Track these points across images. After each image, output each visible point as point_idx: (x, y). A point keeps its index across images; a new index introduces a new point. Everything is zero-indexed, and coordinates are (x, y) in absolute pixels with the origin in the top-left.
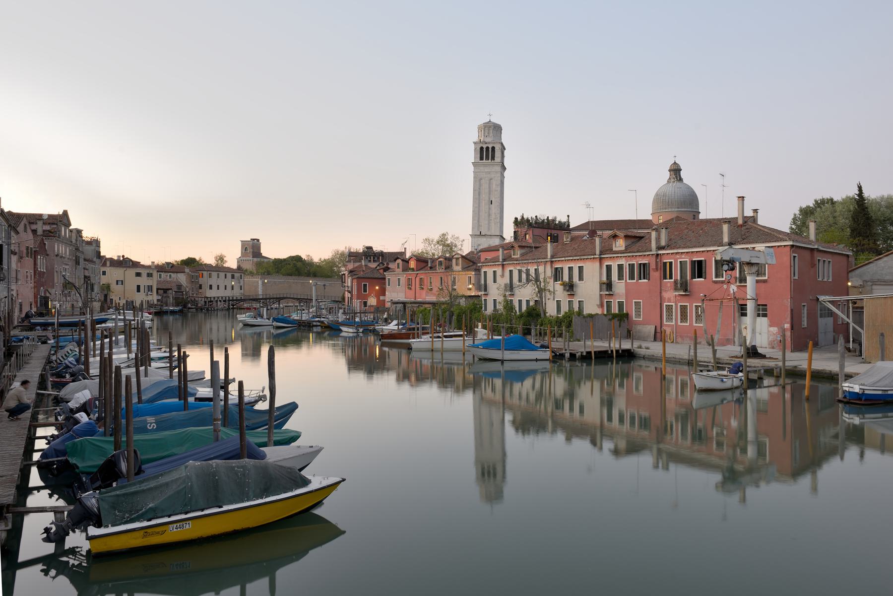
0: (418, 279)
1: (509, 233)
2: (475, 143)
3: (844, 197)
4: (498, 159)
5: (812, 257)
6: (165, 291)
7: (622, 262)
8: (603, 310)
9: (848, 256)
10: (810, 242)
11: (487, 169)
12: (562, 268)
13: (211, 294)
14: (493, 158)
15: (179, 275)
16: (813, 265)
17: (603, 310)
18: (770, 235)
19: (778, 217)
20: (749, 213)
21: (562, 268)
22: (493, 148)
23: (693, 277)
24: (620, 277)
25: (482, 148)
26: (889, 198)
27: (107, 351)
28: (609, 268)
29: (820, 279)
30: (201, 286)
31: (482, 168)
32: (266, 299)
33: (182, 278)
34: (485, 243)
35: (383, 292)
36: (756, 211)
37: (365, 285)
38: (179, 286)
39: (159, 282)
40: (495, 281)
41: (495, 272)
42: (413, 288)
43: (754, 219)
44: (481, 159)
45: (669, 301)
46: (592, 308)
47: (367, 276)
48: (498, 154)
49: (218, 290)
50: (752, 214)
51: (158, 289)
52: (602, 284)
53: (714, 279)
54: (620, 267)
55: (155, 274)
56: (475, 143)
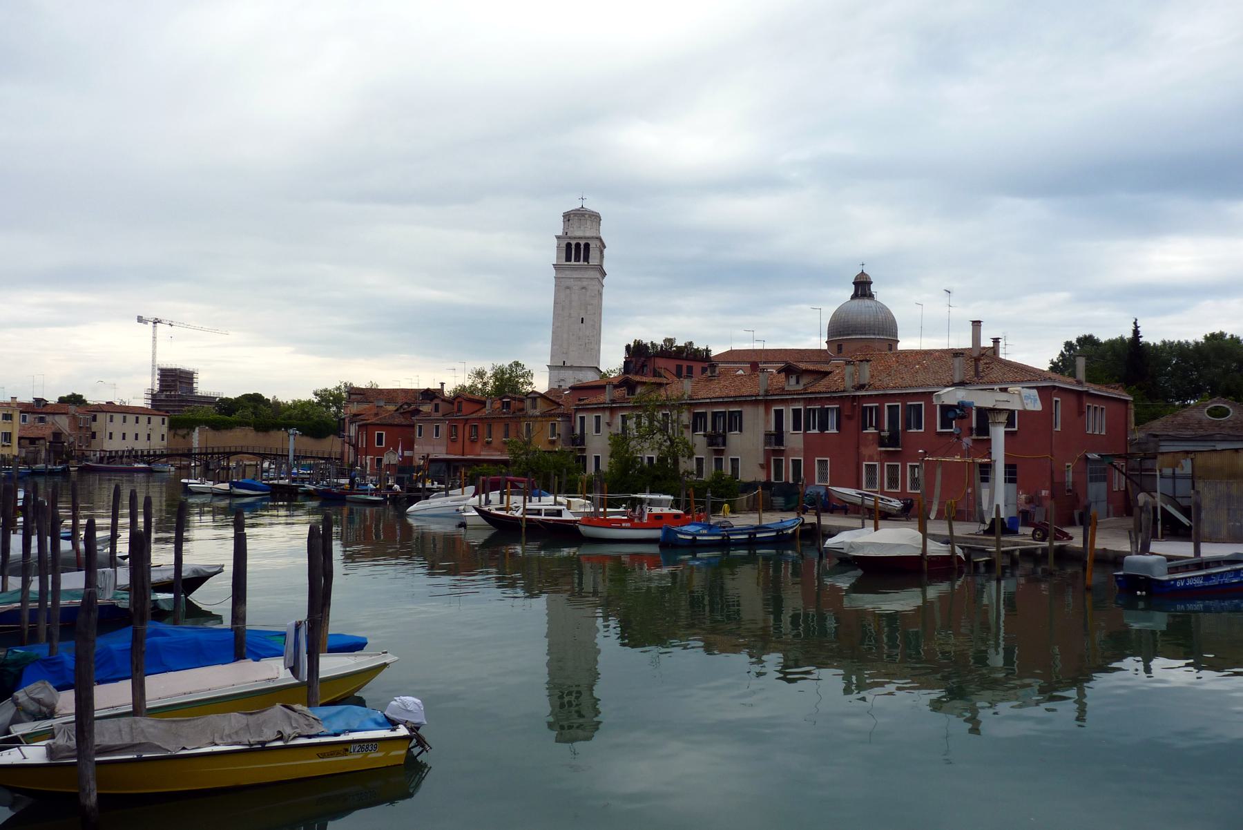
0: (467, 428)
1: (612, 360)
2: (558, 237)
3: (1183, 340)
4: (593, 261)
5: (1080, 405)
6: (33, 441)
7: (800, 406)
8: (768, 475)
9: (1126, 402)
10: (1079, 383)
11: (576, 274)
12: (705, 413)
13: (116, 445)
14: (586, 259)
15: (57, 418)
16: (1081, 413)
17: (768, 475)
18: (1022, 373)
19: (1039, 353)
20: (986, 343)
21: (705, 413)
22: (587, 246)
23: (908, 425)
24: (796, 427)
25: (569, 245)
26: (1234, 340)
27: (141, 520)
28: (779, 414)
29: (1090, 432)
30: (94, 435)
31: (568, 273)
32: (206, 454)
33: (63, 423)
34: (571, 379)
35: (409, 445)
36: (996, 341)
37: (380, 436)
38: (57, 435)
39: (22, 429)
40: (598, 430)
41: (598, 418)
42: (460, 439)
43: (995, 349)
44: (568, 259)
45: (871, 459)
46: (751, 472)
47: (384, 422)
48: (593, 253)
49: (116, 439)
50: (991, 345)
51: (20, 438)
52: (768, 435)
53: (939, 430)
54: (796, 413)
55: (17, 416)
56: (558, 237)
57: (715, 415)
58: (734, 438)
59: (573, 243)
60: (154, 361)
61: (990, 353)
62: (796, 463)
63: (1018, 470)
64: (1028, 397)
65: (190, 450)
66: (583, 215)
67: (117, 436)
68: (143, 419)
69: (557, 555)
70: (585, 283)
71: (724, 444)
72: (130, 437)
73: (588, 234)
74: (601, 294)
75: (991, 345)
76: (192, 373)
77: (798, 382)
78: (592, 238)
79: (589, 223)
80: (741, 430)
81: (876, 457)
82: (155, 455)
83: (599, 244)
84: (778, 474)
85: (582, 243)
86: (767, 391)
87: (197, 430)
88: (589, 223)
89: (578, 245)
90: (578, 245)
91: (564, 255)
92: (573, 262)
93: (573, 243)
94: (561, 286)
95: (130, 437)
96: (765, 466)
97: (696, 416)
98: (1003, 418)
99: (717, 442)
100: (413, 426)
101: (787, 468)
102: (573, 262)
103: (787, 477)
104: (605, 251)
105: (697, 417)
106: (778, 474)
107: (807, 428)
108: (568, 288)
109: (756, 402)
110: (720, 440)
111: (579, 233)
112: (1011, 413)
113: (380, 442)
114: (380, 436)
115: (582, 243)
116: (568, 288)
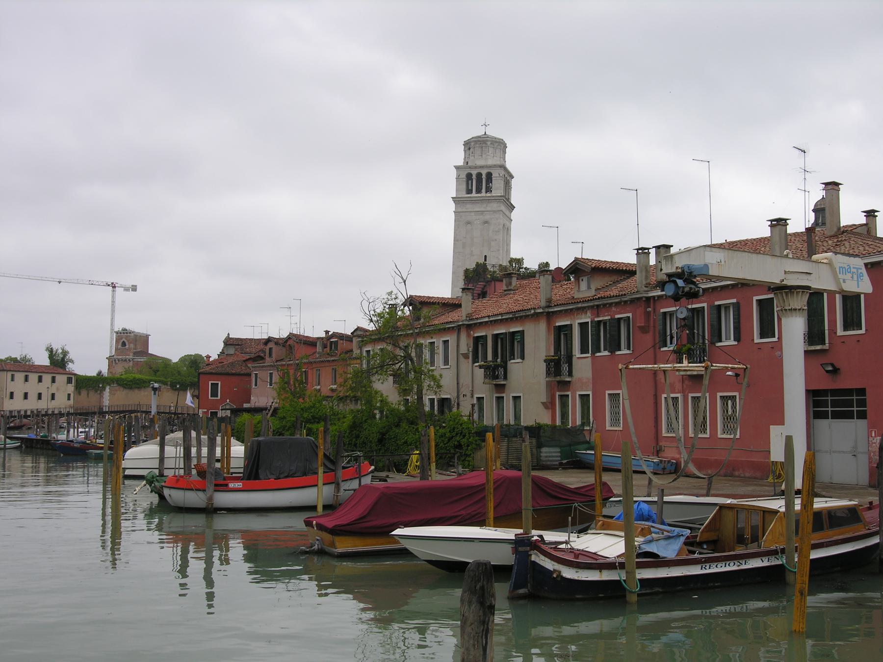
2: (457, 168)
11: (477, 207)
14: (488, 190)
22: (489, 176)
24: (584, 350)
25: (469, 177)
31: (469, 207)
37: (214, 386)
44: (469, 191)
50: (862, 220)
54: (583, 326)
56: (457, 168)
57: (496, 337)
58: (514, 365)
59: (474, 173)
60: (112, 324)
61: (863, 230)
62: (584, 398)
63: (869, 397)
64: (847, 270)
65: (101, 408)
66: (485, 142)
67: (18, 395)
68: (47, 378)
69: (521, 531)
70: (487, 217)
71: (505, 378)
72: (33, 396)
73: (490, 162)
74: (508, 230)
75: (862, 220)
76: (147, 336)
77: (589, 287)
78: (495, 166)
79: (491, 150)
80: (523, 358)
81: (678, 386)
82: (53, 414)
83: (502, 172)
84: (564, 416)
85: (484, 172)
86: (549, 301)
87: (108, 389)
88: (491, 150)
89: (479, 175)
90: (479, 175)
91: (464, 186)
92: (474, 194)
93: (474, 173)
94: (462, 223)
95: (33, 396)
96: (549, 405)
97: (477, 340)
98: (800, 302)
99: (496, 373)
100: (249, 375)
101: (574, 406)
102: (474, 194)
103: (574, 420)
104: (514, 182)
105: (478, 342)
106: (564, 416)
107: (597, 349)
108: (468, 223)
109: (536, 316)
110: (501, 371)
111: (480, 162)
112: (816, 297)
113: (214, 394)
114: (214, 386)
115: (484, 172)
116: (468, 223)
